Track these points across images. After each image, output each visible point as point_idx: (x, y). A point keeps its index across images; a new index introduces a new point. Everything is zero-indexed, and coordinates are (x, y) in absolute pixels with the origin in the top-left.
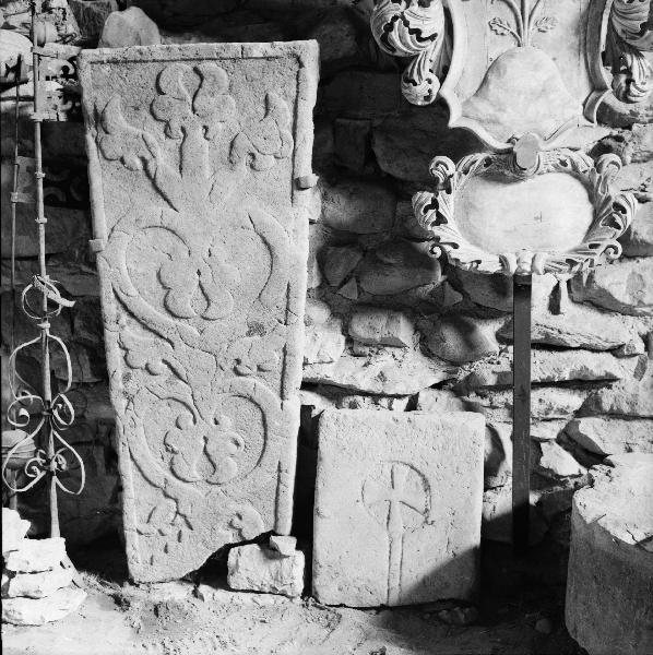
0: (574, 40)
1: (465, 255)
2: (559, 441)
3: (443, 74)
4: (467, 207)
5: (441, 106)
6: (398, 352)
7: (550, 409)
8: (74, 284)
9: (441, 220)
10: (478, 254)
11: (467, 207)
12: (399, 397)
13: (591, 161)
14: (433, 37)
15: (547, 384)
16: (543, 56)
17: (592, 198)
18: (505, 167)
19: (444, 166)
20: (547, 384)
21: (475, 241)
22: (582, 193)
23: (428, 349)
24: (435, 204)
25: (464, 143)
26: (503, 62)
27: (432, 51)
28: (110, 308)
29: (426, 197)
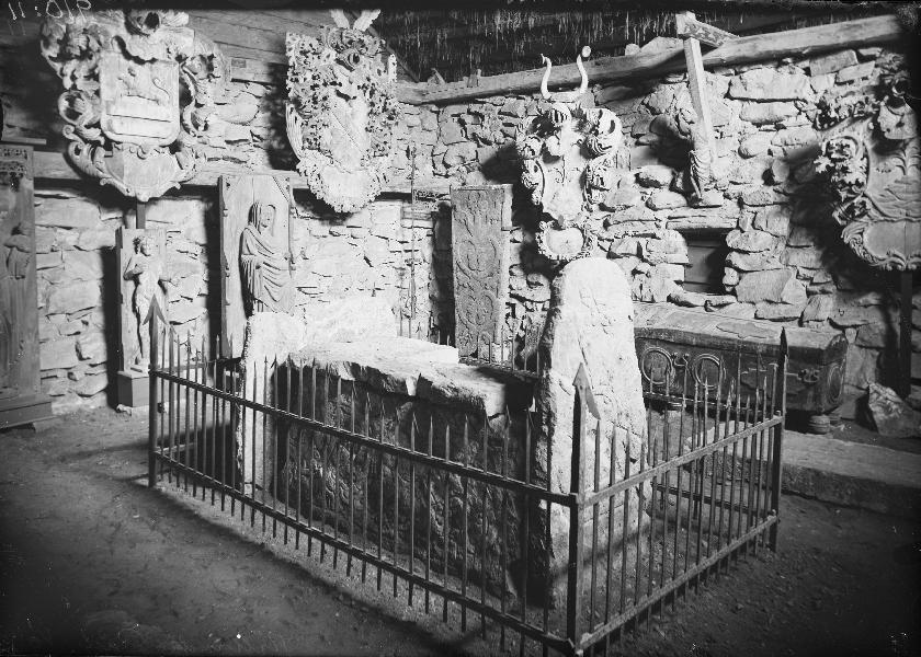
1: (547, 254)
5: (541, 206)
19: (543, 224)
25: (548, 217)
28: (455, 266)
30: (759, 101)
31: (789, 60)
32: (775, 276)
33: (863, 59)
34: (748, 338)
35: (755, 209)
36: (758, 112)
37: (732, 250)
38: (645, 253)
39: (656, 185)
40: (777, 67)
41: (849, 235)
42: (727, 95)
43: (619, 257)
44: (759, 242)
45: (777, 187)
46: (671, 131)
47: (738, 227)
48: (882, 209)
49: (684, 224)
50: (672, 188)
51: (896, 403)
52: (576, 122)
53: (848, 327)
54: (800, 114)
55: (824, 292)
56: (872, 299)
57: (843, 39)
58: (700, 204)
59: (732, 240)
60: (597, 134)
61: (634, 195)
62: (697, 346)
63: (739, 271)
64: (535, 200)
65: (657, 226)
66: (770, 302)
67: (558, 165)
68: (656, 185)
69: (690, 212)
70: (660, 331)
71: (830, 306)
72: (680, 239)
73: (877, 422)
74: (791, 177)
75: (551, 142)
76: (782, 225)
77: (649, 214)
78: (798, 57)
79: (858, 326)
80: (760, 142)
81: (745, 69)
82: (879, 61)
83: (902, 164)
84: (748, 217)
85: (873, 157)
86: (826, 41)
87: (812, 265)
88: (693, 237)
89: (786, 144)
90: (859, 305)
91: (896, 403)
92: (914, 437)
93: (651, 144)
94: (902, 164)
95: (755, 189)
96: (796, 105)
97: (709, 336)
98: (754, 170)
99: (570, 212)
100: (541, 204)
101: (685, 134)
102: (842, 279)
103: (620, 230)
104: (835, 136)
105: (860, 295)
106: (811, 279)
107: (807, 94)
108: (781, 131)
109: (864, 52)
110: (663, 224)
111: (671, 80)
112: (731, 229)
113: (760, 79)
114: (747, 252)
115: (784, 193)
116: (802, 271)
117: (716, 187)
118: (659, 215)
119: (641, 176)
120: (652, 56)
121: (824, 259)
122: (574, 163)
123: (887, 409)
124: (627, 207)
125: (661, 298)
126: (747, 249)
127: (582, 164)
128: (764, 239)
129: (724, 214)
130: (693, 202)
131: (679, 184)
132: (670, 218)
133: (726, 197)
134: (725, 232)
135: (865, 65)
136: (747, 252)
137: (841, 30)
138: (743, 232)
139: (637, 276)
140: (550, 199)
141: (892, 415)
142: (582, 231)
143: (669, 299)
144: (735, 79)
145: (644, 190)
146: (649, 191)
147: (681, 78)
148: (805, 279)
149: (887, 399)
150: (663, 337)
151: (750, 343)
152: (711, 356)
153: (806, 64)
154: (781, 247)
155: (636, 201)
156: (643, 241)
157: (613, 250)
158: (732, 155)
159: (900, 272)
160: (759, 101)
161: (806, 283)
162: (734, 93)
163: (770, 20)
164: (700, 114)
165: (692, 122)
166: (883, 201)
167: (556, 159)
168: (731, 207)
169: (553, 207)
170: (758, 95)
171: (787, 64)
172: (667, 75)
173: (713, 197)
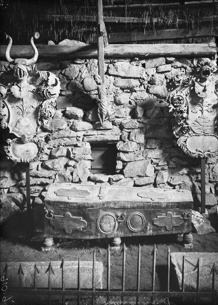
0: (34, 116)
1: (14, 158)
2: (39, 197)
3: (8, 122)
4: (14, 149)
5: (8, 129)
6: (6, 179)
7: (35, 190)
8: (22, 149)
9: (9, 152)
10: (16, 158)
11: (14, 149)
12: (6, 188)
13: (136, 121)
14: (5, 115)
15: (35, 185)
16: (28, 119)
17: (38, 147)
18: (21, 141)
19: (10, 141)
20: (35, 185)
21: (16, 156)
22: (36, 146)
23: (13, 178)
24: (7, 149)
25: (13, 136)
26: (20, 120)
27: (6, 118)
29: (6, 147)
30: (123, 78)
31: (137, 59)
32: (141, 164)
33: (167, 62)
34: (156, 201)
35: (129, 130)
36: (122, 83)
37: (120, 151)
38: (72, 156)
39: (76, 117)
40: (130, 62)
41: (181, 141)
42: (107, 73)
43: (57, 158)
44: (133, 147)
45: (139, 120)
46: (80, 89)
47: (121, 139)
48: (194, 130)
49: (93, 138)
50: (85, 119)
51: (201, 218)
52: (30, 78)
53: (176, 185)
54: (141, 85)
55: (163, 169)
56: (185, 171)
57: (162, 52)
58: (101, 128)
59: (120, 146)
60: (47, 85)
61: (64, 124)
62: (130, 209)
63: (123, 161)
64: (4, 125)
65: (78, 140)
66: (140, 176)
67: (19, 104)
68: (76, 117)
69: (95, 132)
70: (107, 203)
71: (167, 176)
72: (88, 146)
73: (196, 228)
74: (145, 115)
75: (15, 89)
76: (141, 138)
77: (73, 133)
78: (142, 57)
79: (180, 184)
80: (124, 98)
81: (116, 61)
82: (173, 64)
83: (201, 109)
84: (126, 134)
85: (190, 106)
86: (156, 52)
87: (158, 157)
88: (95, 145)
89: (136, 99)
90: (179, 174)
91: (201, 218)
92: (211, 233)
93: (68, 96)
94: (201, 109)
95: (127, 120)
96: (140, 81)
97: (137, 202)
98: (126, 111)
99: (29, 133)
100: (7, 127)
101: (87, 91)
102: (171, 163)
103: (57, 142)
104: (175, 94)
105: (180, 170)
106: (158, 164)
107: (144, 76)
108: (133, 93)
109: (168, 59)
110: (81, 139)
111: (78, 62)
112: (118, 141)
113: (123, 66)
114: (127, 152)
115: (143, 123)
116: (154, 161)
117: (108, 120)
118: (79, 134)
119: (67, 112)
120: (68, 47)
121: (163, 154)
122: (30, 104)
123: (198, 221)
124: (60, 130)
125: (84, 180)
126: (128, 150)
127: (36, 104)
128: (133, 146)
129: (114, 133)
130: (97, 126)
131: (90, 117)
132: (84, 136)
133: (114, 124)
134: (114, 143)
135: (168, 65)
136: (127, 152)
137: (162, 47)
138: (124, 142)
139: (68, 168)
140: (14, 125)
141: (201, 224)
142: (37, 145)
143: (89, 179)
144: (111, 66)
145: (68, 120)
146: (72, 121)
147: (83, 61)
148: (155, 164)
149: (197, 217)
150: (112, 206)
151: (158, 203)
152: (138, 213)
153: (144, 62)
154: (142, 149)
155: (65, 126)
156: (70, 148)
157: (54, 154)
158: (111, 103)
159: (201, 158)
160: (123, 78)
161: (155, 166)
162: (111, 72)
163: (120, 39)
164: (103, 82)
165: (100, 84)
166: (194, 126)
167: (19, 99)
168: (116, 129)
169: (17, 130)
170: (123, 74)
171: (135, 60)
172: (76, 58)
173: (108, 125)
